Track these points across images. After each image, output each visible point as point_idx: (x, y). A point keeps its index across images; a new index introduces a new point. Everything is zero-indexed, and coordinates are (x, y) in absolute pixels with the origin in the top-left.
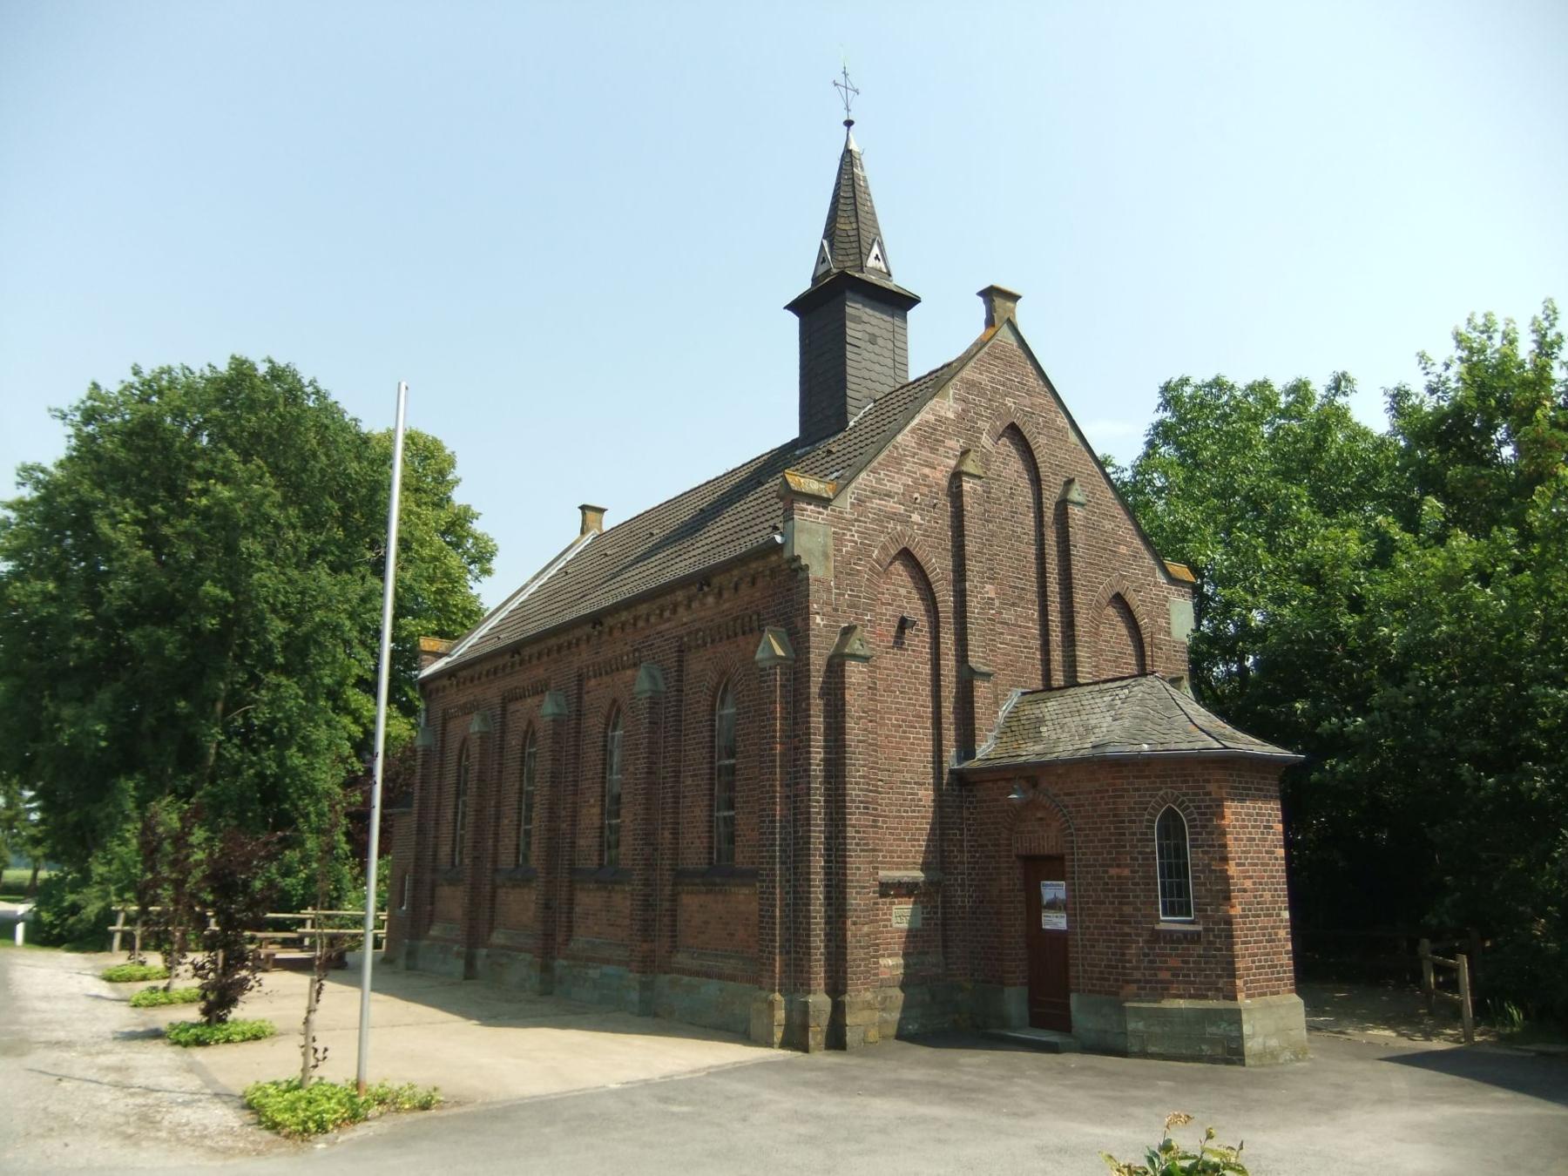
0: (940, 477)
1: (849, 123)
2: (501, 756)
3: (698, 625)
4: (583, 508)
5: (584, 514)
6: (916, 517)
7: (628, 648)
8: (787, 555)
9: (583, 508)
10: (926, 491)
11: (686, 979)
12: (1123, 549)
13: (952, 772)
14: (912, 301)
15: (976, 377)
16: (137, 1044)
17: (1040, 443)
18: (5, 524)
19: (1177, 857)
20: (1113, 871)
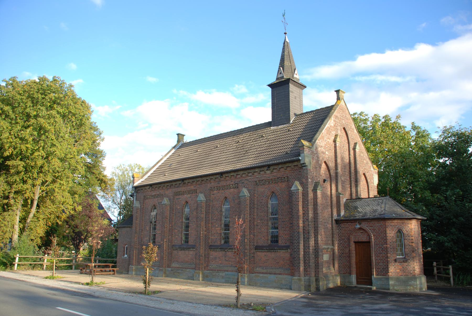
0: (331, 141)
1: (285, 33)
2: (332, 232)
3: (263, 178)
4: (178, 134)
5: (178, 136)
6: (327, 153)
7: (233, 183)
8: (302, 162)
9: (178, 134)
10: (328, 145)
11: (261, 275)
12: (365, 161)
13: (335, 220)
14: (306, 87)
15: (337, 115)
16: (220, 309)
17: (349, 132)
18: (471, 211)
19: (400, 242)
20: (385, 246)
